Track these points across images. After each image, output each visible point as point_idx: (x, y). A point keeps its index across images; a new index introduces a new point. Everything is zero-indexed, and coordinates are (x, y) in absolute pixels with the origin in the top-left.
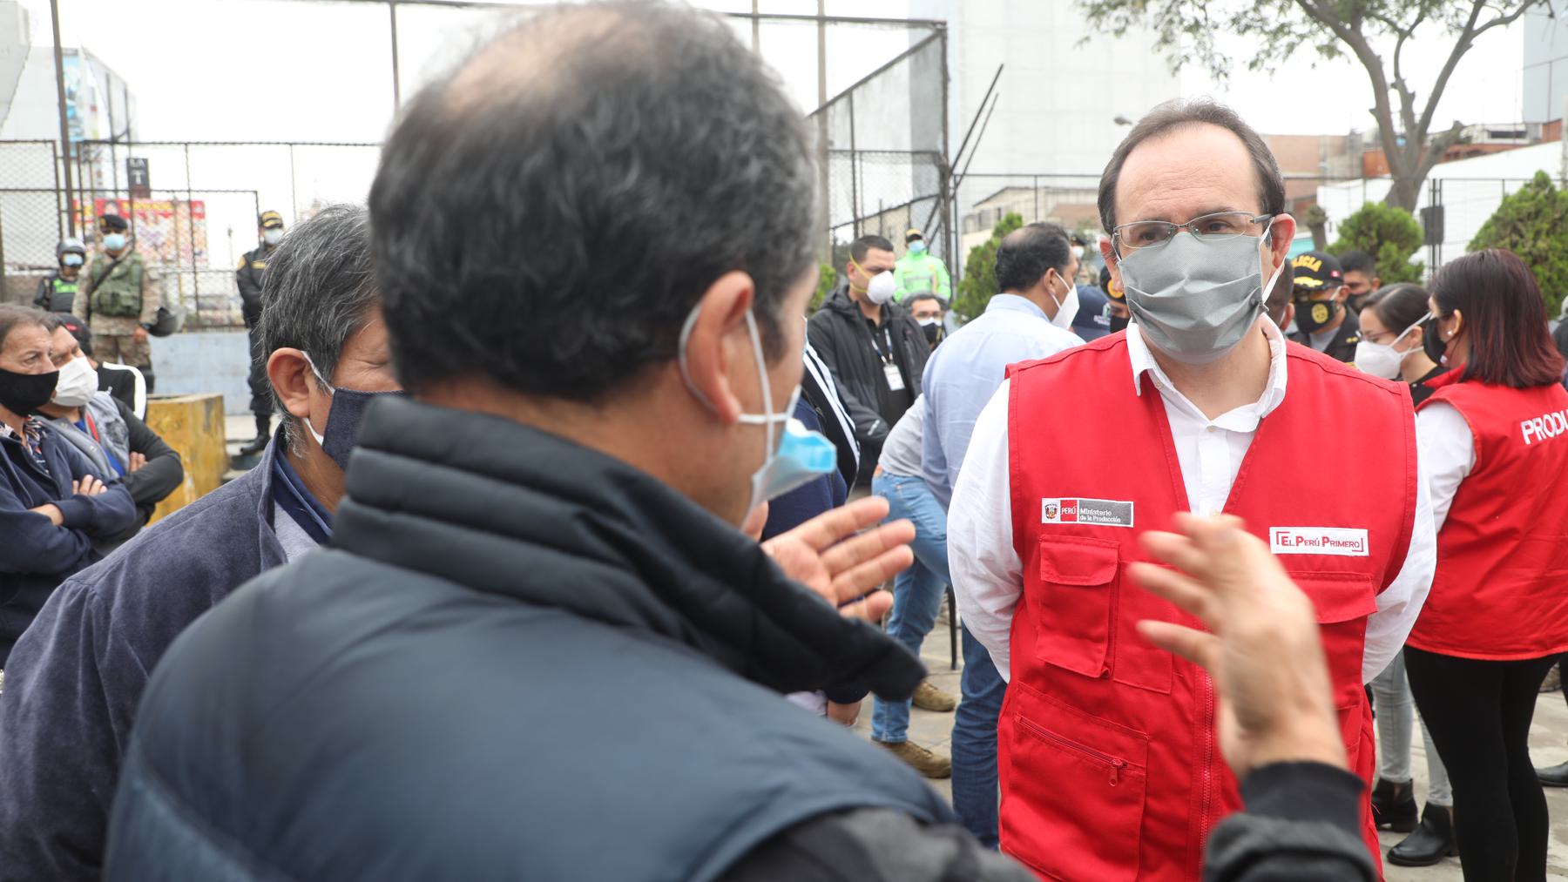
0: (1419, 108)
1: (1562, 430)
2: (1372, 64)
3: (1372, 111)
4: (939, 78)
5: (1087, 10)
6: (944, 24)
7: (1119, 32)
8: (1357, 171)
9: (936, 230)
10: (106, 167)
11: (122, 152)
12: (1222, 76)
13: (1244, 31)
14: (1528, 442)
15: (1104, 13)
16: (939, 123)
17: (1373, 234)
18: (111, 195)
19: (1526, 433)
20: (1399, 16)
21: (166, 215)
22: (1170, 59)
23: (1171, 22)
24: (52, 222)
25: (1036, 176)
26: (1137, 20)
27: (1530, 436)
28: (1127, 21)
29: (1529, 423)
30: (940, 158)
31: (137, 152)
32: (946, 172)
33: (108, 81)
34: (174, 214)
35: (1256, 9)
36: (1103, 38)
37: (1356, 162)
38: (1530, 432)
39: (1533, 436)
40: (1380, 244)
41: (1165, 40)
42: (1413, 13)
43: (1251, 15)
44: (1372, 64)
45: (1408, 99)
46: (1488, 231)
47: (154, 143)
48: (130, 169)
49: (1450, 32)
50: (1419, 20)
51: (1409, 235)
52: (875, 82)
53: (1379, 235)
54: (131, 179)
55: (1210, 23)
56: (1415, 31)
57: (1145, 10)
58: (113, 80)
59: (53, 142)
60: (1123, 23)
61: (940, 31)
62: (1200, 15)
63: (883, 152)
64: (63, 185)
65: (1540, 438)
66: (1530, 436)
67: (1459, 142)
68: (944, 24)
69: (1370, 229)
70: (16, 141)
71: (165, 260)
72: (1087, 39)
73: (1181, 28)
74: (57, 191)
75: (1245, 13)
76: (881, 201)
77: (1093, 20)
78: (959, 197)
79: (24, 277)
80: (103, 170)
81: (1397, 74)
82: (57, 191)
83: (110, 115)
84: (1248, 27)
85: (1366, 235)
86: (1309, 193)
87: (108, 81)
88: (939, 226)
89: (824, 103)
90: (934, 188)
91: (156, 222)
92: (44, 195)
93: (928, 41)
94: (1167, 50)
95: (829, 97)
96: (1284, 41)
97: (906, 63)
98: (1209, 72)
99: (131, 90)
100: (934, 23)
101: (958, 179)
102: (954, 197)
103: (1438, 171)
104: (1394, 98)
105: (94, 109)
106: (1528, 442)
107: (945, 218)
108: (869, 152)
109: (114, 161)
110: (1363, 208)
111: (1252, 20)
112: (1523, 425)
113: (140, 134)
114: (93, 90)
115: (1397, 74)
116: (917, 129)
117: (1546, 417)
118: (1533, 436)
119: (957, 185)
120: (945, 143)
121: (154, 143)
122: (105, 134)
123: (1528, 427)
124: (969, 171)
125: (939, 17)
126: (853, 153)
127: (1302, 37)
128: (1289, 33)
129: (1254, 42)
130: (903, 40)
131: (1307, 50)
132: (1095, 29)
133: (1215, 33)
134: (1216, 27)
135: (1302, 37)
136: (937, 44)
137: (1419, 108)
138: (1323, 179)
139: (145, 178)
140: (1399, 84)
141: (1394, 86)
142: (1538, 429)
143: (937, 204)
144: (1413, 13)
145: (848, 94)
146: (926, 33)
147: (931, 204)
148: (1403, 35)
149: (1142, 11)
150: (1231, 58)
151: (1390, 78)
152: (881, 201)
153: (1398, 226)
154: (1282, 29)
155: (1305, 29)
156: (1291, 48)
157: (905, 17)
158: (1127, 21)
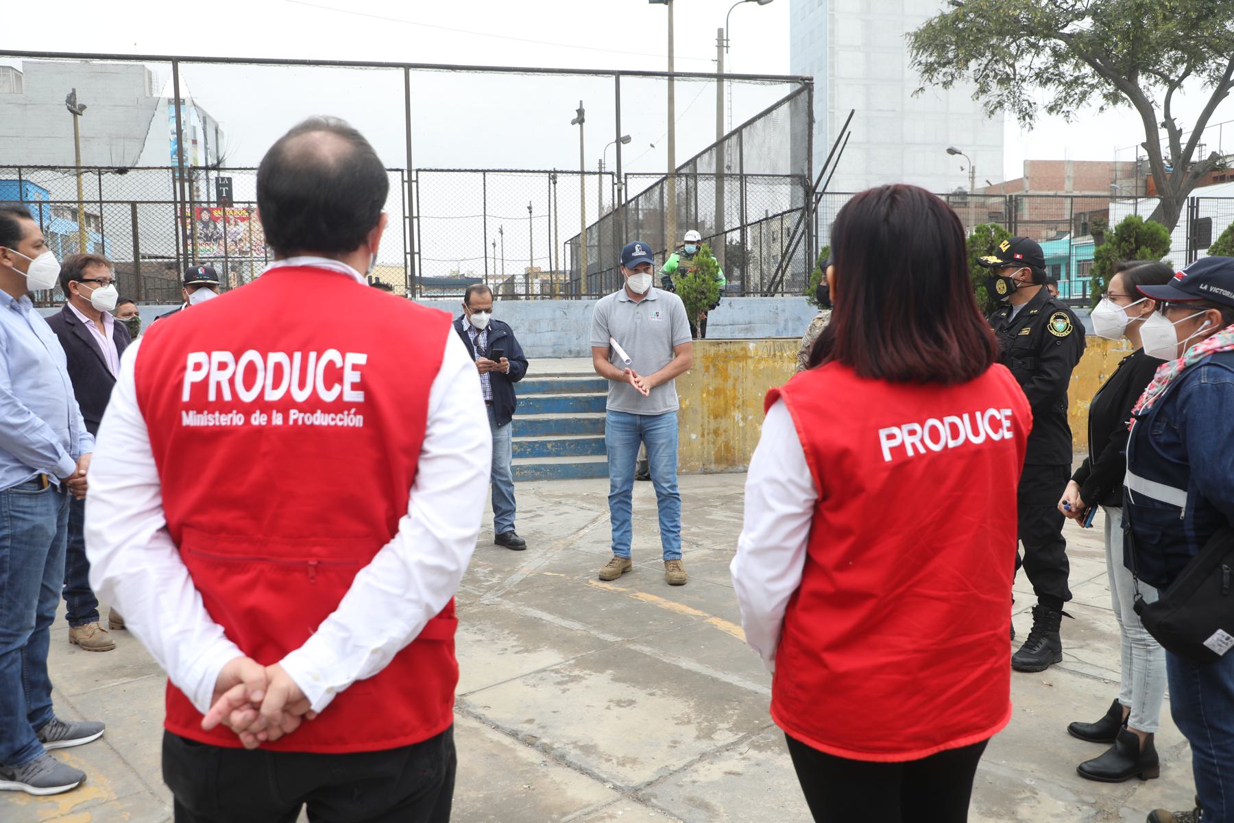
0: (1184, 140)
1: (961, 440)
2: (1146, 110)
3: (1143, 145)
4: (805, 119)
5: (922, 68)
6: (811, 79)
7: (946, 85)
8: (1141, 191)
9: (801, 236)
10: (202, 185)
11: (213, 174)
12: (1027, 117)
13: (1046, 83)
14: (888, 457)
15: (935, 70)
16: (805, 155)
17: (1132, 240)
18: (205, 205)
19: (886, 445)
20: (1171, 72)
21: (243, 220)
22: (986, 104)
23: (987, 76)
24: (171, 225)
25: (20, 168)
26: (961, 75)
27: (892, 450)
28: (952, 75)
29: (895, 430)
30: (805, 180)
31: (223, 174)
32: (810, 191)
33: (205, 122)
34: (249, 218)
35: (1056, 66)
36: (934, 90)
37: (1140, 183)
38: (895, 443)
39: (899, 451)
40: (1138, 248)
41: (983, 90)
42: (1182, 69)
43: (1051, 70)
44: (1146, 110)
45: (1175, 135)
46: (1226, 239)
47: (240, 169)
48: (218, 185)
49: (1212, 83)
50: (1186, 74)
51: (1160, 241)
52: (759, 123)
53: (1136, 241)
54: (219, 193)
55: (1018, 77)
56: (1183, 83)
57: (968, 69)
58: (207, 119)
59: (402, 171)
60: (950, 78)
61: (806, 85)
62: (1009, 70)
63: (763, 175)
64: (179, 199)
65: (910, 453)
66: (892, 450)
67: (1215, 169)
68: (811, 79)
69: (1130, 237)
70: (149, 168)
71: (241, 252)
72: (922, 89)
73: (995, 81)
74: (175, 202)
75: (1047, 69)
76: (767, 211)
77: (926, 75)
78: (820, 210)
79: (152, 263)
80: (201, 188)
81: (1167, 115)
82: (175, 202)
83: (206, 148)
84: (1049, 80)
85: (1127, 241)
86: (1104, 207)
87: (205, 122)
88: (803, 233)
89: (720, 138)
90: (801, 204)
91: (236, 224)
92: (166, 206)
93: (799, 92)
94: (983, 98)
95: (726, 132)
96: (1079, 90)
97: (786, 106)
98: (1016, 115)
99: (220, 128)
100: (803, 79)
101: (819, 196)
102: (815, 210)
103: (1196, 193)
104: (1163, 134)
105: (195, 142)
106: (888, 457)
107: (808, 226)
108: (752, 175)
109: (208, 179)
110: (1125, 221)
111: (1052, 74)
112: (883, 433)
113: (228, 163)
114: (194, 127)
115: (1167, 115)
116: (794, 162)
117: (932, 422)
118: (899, 451)
119: (818, 201)
120: (810, 169)
121: (240, 169)
122: (202, 164)
123: (891, 437)
124: (828, 190)
125: (807, 75)
126: (742, 177)
127: (1093, 87)
128: (1083, 83)
129: (1051, 93)
130: (786, 89)
131: (1096, 98)
132: (928, 81)
133: (1024, 85)
134: (1023, 80)
135: (1093, 87)
136: (805, 94)
137: (1184, 140)
138: (1113, 198)
139: (230, 193)
140: (1169, 123)
141: (1164, 125)
142: (909, 441)
143: (802, 215)
144: (1182, 69)
145: (738, 131)
146: (798, 86)
147: (798, 215)
148: (1173, 85)
149: (965, 68)
150: (1035, 103)
151: (1160, 117)
152: (767, 211)
153: (1152, 234)
154: (1076, 81)
155: (1095, 81)
156: (1084, 95)
157: (787, 73)
158: (952, 75)
